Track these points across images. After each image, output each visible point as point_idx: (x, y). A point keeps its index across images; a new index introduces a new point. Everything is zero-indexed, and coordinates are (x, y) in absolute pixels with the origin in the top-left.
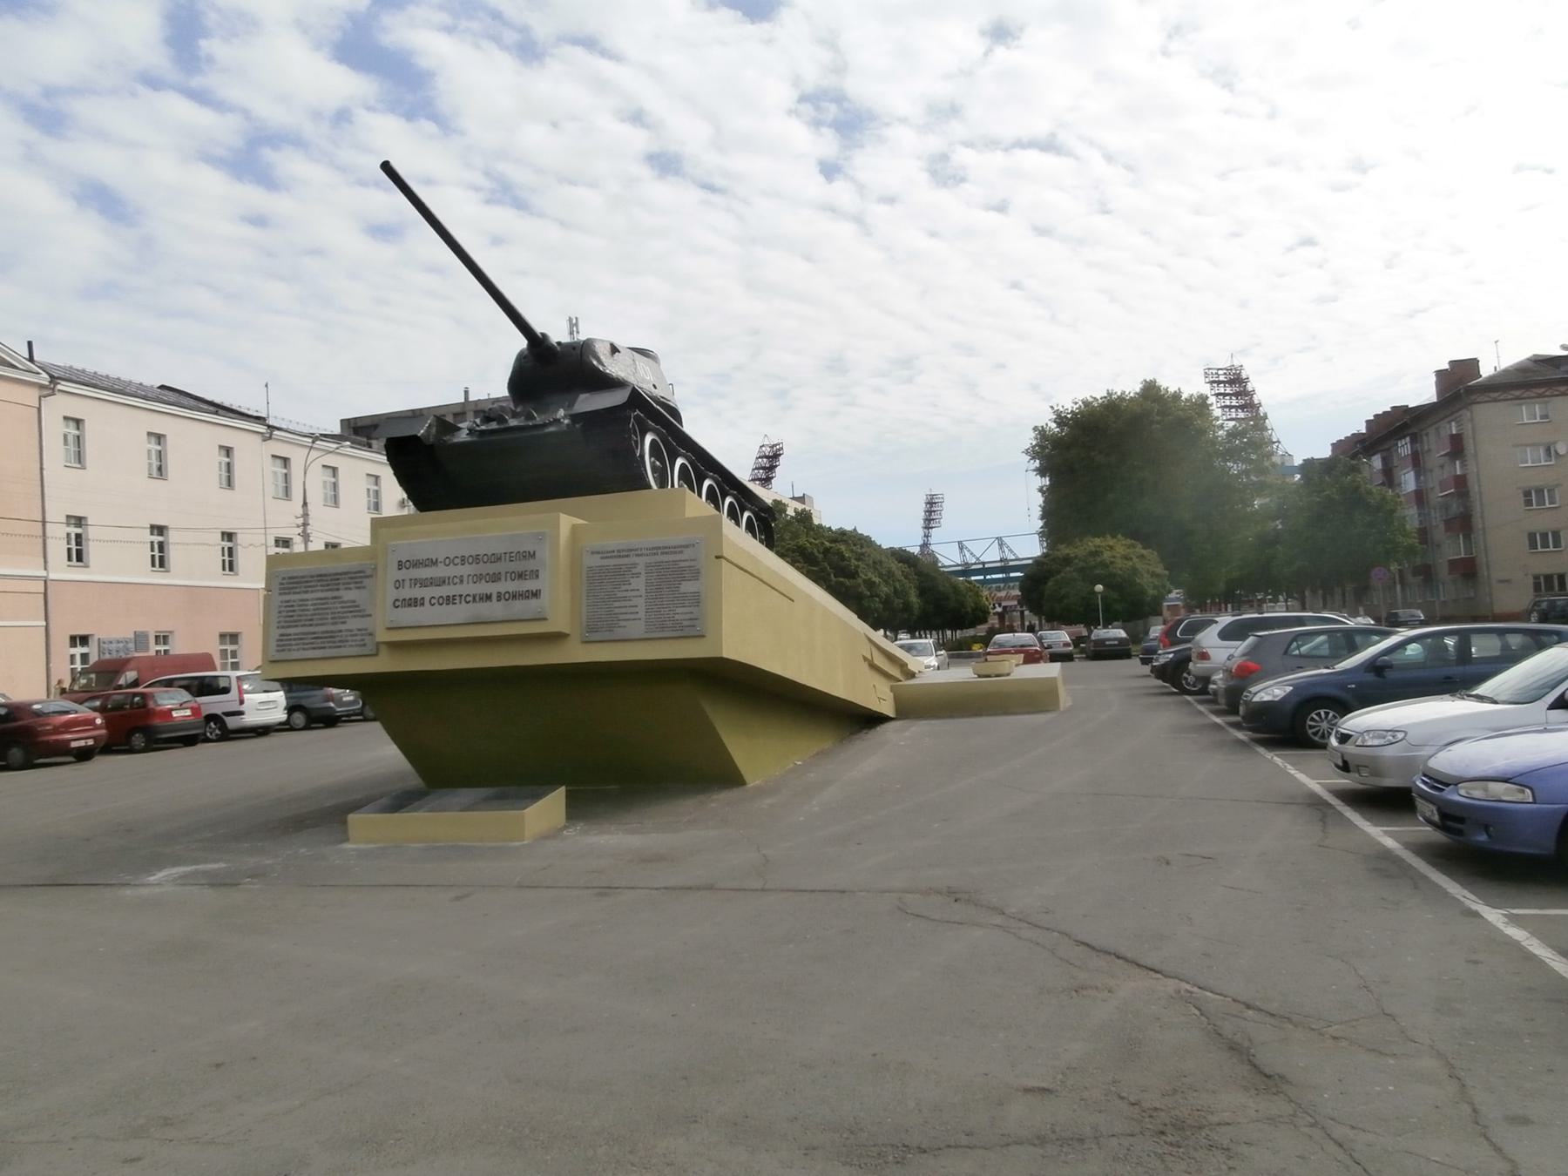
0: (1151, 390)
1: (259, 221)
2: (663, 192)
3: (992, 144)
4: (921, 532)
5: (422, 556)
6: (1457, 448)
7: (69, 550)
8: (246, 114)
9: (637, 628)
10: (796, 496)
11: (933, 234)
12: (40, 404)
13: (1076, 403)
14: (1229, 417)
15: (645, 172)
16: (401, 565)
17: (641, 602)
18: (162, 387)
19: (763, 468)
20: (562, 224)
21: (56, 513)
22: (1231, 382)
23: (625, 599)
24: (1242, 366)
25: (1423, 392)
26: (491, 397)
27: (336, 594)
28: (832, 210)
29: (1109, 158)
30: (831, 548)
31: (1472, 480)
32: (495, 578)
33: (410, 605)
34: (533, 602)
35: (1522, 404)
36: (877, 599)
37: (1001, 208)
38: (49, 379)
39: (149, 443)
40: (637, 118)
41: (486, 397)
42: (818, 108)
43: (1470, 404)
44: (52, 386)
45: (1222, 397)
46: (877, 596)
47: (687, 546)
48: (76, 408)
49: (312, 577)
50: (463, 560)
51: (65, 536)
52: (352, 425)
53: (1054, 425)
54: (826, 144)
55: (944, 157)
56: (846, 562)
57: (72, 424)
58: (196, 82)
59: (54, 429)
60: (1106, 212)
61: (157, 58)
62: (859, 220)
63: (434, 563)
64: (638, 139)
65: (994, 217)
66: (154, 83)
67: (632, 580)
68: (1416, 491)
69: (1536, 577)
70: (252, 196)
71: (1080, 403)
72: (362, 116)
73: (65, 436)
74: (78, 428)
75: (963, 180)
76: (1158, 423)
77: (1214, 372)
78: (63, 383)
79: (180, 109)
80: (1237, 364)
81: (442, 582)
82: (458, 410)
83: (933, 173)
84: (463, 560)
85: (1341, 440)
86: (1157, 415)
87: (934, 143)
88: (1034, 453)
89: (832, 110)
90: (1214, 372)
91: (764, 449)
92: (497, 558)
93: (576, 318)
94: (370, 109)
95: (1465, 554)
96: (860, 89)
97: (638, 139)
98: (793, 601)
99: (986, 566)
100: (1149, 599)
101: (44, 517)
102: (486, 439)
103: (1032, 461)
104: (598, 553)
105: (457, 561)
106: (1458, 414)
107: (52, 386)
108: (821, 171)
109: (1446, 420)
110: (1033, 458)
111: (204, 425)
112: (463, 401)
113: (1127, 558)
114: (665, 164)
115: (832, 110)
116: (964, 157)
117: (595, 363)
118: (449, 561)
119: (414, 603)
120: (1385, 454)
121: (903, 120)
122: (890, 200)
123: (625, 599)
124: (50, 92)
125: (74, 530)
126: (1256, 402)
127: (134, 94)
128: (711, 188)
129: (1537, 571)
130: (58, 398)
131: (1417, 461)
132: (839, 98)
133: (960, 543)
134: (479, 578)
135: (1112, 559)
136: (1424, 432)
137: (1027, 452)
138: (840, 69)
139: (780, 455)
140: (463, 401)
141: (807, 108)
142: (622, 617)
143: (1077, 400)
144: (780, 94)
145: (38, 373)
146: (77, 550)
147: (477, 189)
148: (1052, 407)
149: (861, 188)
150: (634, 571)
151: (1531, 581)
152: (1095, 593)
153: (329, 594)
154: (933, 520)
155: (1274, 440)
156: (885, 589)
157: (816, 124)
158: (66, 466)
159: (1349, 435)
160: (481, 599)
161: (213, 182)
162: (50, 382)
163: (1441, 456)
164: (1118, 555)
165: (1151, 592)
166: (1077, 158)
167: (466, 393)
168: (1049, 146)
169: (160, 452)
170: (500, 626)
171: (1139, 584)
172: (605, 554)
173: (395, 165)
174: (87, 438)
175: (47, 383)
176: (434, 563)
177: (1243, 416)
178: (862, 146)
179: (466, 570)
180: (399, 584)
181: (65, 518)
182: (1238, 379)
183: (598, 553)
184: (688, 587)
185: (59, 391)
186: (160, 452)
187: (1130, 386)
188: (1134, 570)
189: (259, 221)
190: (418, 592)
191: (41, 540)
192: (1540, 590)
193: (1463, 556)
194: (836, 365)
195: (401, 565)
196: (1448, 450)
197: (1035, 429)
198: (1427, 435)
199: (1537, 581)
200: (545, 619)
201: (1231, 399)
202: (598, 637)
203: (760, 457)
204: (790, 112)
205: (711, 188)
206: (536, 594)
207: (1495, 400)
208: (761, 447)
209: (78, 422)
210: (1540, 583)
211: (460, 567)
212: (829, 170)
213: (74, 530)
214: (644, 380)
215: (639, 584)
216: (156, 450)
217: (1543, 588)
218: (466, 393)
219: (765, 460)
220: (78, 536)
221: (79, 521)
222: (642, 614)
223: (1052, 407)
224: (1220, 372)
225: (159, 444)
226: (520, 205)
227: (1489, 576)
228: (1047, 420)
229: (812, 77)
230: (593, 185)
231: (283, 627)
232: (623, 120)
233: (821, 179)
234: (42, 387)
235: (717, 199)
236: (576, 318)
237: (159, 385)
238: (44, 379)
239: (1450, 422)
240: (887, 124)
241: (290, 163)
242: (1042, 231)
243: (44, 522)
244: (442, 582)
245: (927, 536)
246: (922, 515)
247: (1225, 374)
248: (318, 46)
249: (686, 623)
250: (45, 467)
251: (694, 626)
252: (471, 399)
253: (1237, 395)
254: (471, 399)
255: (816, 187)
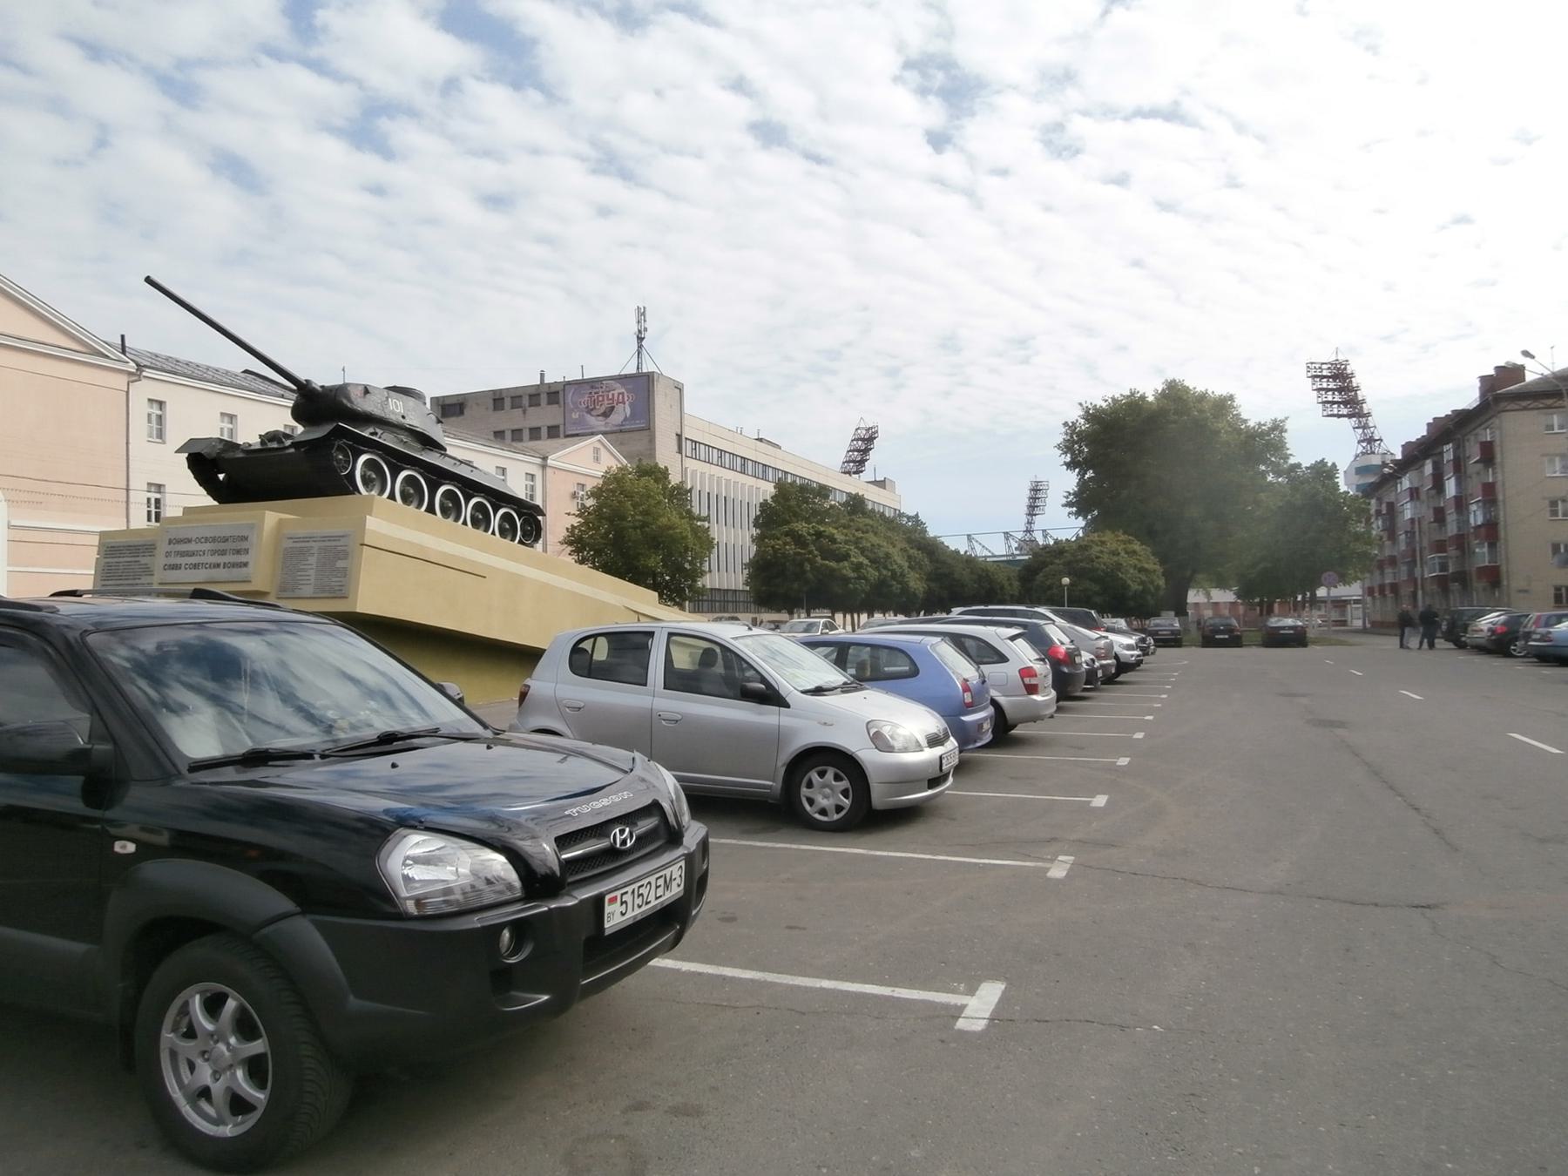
0: (1175, 394)
1: (378, 190)
2: (768, 162)
3: (1109, 112)
4: (1024, 519)
5: (182, 536)
6: (1488, 456)
7: (149, 512)
8: (360, 84)
9: (308, 590)
10: (878, 479)
11: (1048, 209)
12: (128, 388)
13: (1106, 401)
14: (1330, 413)
15: (749, 141)
16: (170, 542)
17: (312, 572)
18: (246, 371)
19: (858, 451)
20: (668, 195)
21: (139, 483)
22: (1334, 377)
23: (304, 570)
24: (1347, 361)
25: (1469, 398)
26: (566, 380)
27: (137, 559)
28: (940, 182)
29: (1240, 128)
30: (824, 531)
31: (1499, 487)
32: (223, 553)
33: (173, 569)
34: (244, 569)
35: (1552, 414)
36: (863, 581)
37: (1122, 180)
38: (136, 367)
39: (223, 422)
40: (739, 86)
41: (562, 380)
42: (924, 75)
43: (1499, 412)
44: (139, 373)
45: (1324, 393)
46: (865, 578)
47: (343, 536)
48: (159, 392)
49: (124, 547)
50: (206, 540)
51: (146, 502)
52: (441, 403)
53: (1082, 421)
54: (933, 114)
55: (1059, 127)
56: (837, 545)
57: (155, 406)
58: (314, 52)
59: (140, 409)
60: (1236, 186)
61: (274, 28)
62: (969, 193)
63: (189, 541)
64: (740, 109)
65: (1113, 189)
66: (276, 54)
67: (309, 558)
68: (1455, 497)
69: (1558, 589)
70: (370, 165)
71: (1110, 400)
72: (471, 85)
73: (149, 415)
74: (161, 409)
75: (1078, 152)
76: (1175, 422)
77: (1317, 366)
78: (147, 370)
79: (302, 80)
80: (1341, 358)
81: (193, 554)
82: (533, 391)
83: (1048, 143)
84: (206, 540)
85: (1410, 442)
86: (1174, 414)
87: (1048, 112)
88: (1067, 447)
89: (939, 78)
90: (1317, 366)
91: (859, 431)
92: (226, 540)
93: (644, 308)
94: (478, 78)
95: (1489, 562)
96: (972, 55)
97: (740, 109)
98: (485, 577)
99: (988, 559)
100: (1130, 594)
101: (128, 485)
102: (250, 456)
103: (1063, 456)
104: (291, 538)
105: (203, 540)
106: (1489, 423)
107: (139, 373)
108: (929, 142)
109: (1483, 426)
110: (1066, 453)
111: (271, 406)
112: (539, 383)
113: (1115, 553)
114: (769, 133)
115: (939, 78)
116: (1080, 126)
117: (345, 401)
118: (199, 540)
119: (176, 567)
120: (1436, 458)
121: (1015, 88)
122: (1003, 172)
123: (304, 570)
124: (182, 64)
125: (154, 496)
126: (1360, 398)
127: (258, 65)
128: (818, 160)
129: (1559, 582)
130: (144, 381)
131: (1459, 466)
132: (947, 65)
133: (969, 536)
134: (214, 552)
135: (1098, 554)
136: (1466, 438)
137: (1059, 447)
138: (948, 34)
139: (875, 438)
140: (539, 383)
141: (913, 76)
142: (301, 582)
143: (1106, 398)
144: (885, 60)
145: (128, 362)
146: (156, 512)
147: (583, 159)
148: (1081, 404)
149: (972, 161)
150: (312, 552)
151: (1552, 592)
152: (1061, 586)
153: (133, 559)
154: (1037, 507)
155: (1377, 438)
156: (872, 574)
157: (923, 92)
158: (149, 441)
159: (1419, 437)
160: (214, 567)
161: (334, 151)
162: (137, 370)
163: (1475, 462)
164: (1105, 550)
165: (1135, 587)
166: (1202, 128)
167: (542, 375)
168: (1172, 115)
169: (232, 430)
170: (238, 584)
171: (1121, 578)
172: (296, 539)
173: (155, 278)
174: (167, 417)
175: (134, 371)
176: (189, 541)
177: (1345, 413)
178: (973, 114)
179: (207, 546)
180: (168, 554)
181: (146, 486)
182: (1342, 374)
183: (291, 538)
184: (340, 564)
185: (145, 377)
186: (232, 430)
187: (1150, 388)
188: (1119, 566)
189: (378, 190)
190: (179, 560)
191: (125, 505)
192: (1561, 602)
193: (1487, 564)
194: (949, 343)
195: (170, 542)
196: (1478, 458)
197: (1066, 424)
198: (1468, 440)
199: (1558, 592)
200: (250, 581)
201: (1334, 394)
202: (286, 595)
203: (854, 440)
204: (897, 79)
205: (818, 160)
206: (245, 565)
207: (1525, 409)
208: (857, 429)
209: (161, 404)
210: (1561, 595)
211: (204, 544)
212: (938, 141)
213: (154, 496)
214: (393, 412)
215: (313, 560)
216: (228, 429)
217: (1564, 600)
218: (542, 375)
219: (860, 443)
220: (158, 501)
221: (159, 488)
222: (312, 581)
223: (1081, 404)
224: (1324, 367)
225: (231, 423)
226: (626, 175)
227: (1508, 586)
228: (1075, 415)
229: (917, 42)
230: (699, 155)
231: (105, 580)
232: (724, 88)
233: (929, 149)
234: (130, 374)
235: (822, 170)
236: (644, 308)
237: (243, 370)
238: (133, 368)
239: (1485, 429)
240: (998, 92)
241: (403, 133)
242: (1165, 207)
243: (128, 490)
244: (193, 554)
245: (1030, 523)
246: (1026, 502)
247: (1329, 368)
248: (425, 14)
249: (337, 588)
250: (131, 441)
251: (341, 590)
252: (546, 382)
253: (1340, 390)
254: (546, 382)
255: (924, 158)
